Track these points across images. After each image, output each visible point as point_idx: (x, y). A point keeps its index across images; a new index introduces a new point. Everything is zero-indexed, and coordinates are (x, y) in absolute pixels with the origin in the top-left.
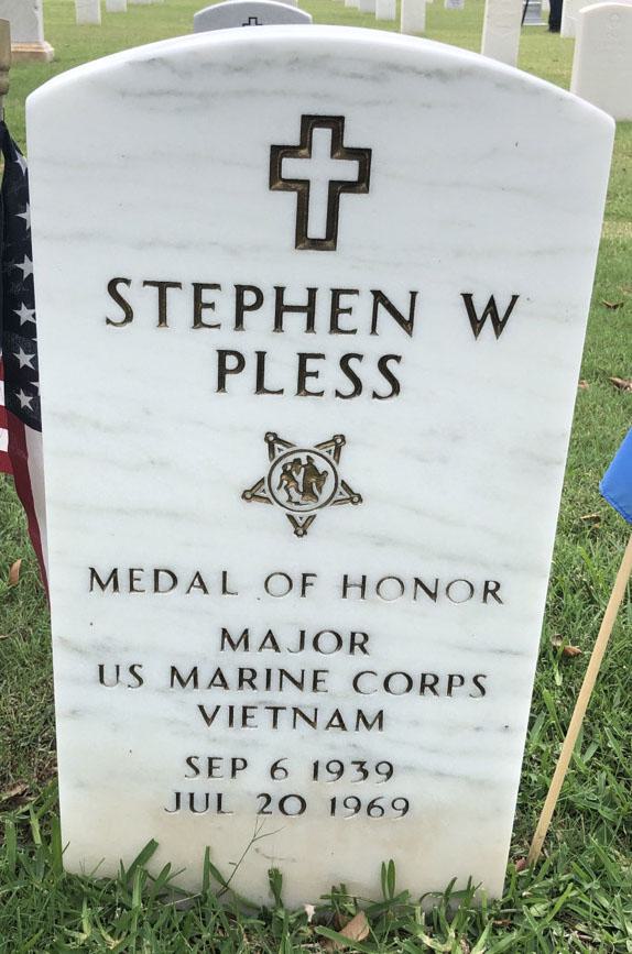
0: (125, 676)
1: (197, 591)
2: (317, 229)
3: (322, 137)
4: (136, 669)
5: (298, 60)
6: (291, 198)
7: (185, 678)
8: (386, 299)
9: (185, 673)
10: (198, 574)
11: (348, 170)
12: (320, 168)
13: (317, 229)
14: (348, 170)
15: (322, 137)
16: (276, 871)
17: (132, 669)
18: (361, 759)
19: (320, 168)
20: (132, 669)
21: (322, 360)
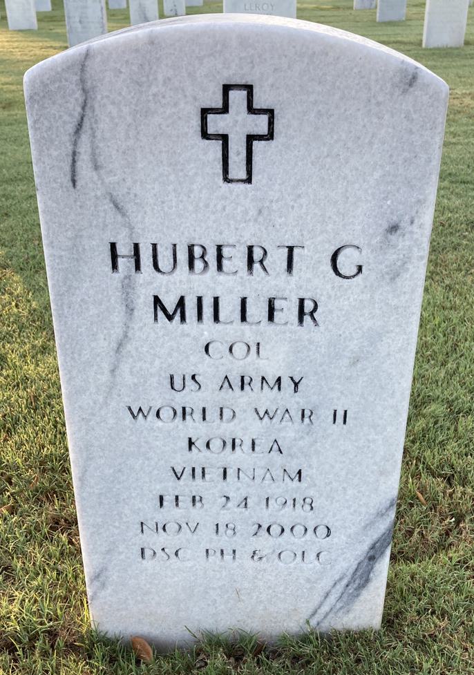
0: (189, 382)
1: (275, 453)
2: (237, 170)
3: (238, 98)
4: (196, 378)
5: (219, 43)
6: (217, 146)
7: (170, 311)
8: (273, 118)
9: (170, 304)
10: (226, 377)
11: (260, 124)
12: (237, 124)
13: (237, 170)
14: (260, 124)
15: (238, 98)
16: (218, 270)
17: (193, 377)
18: (261, 524)
19: (237, 124)
20: (193, 377)
21: (248, 300)
